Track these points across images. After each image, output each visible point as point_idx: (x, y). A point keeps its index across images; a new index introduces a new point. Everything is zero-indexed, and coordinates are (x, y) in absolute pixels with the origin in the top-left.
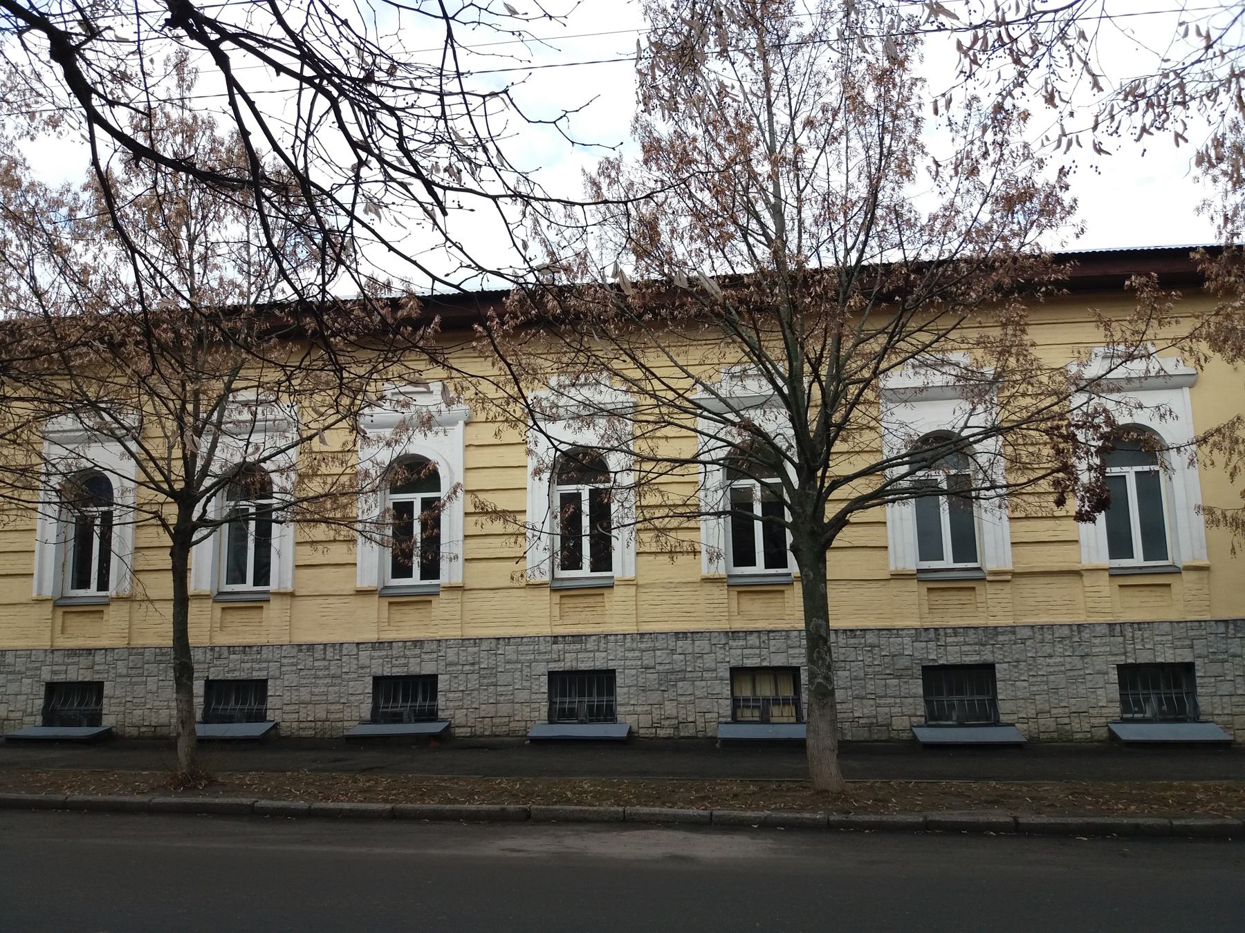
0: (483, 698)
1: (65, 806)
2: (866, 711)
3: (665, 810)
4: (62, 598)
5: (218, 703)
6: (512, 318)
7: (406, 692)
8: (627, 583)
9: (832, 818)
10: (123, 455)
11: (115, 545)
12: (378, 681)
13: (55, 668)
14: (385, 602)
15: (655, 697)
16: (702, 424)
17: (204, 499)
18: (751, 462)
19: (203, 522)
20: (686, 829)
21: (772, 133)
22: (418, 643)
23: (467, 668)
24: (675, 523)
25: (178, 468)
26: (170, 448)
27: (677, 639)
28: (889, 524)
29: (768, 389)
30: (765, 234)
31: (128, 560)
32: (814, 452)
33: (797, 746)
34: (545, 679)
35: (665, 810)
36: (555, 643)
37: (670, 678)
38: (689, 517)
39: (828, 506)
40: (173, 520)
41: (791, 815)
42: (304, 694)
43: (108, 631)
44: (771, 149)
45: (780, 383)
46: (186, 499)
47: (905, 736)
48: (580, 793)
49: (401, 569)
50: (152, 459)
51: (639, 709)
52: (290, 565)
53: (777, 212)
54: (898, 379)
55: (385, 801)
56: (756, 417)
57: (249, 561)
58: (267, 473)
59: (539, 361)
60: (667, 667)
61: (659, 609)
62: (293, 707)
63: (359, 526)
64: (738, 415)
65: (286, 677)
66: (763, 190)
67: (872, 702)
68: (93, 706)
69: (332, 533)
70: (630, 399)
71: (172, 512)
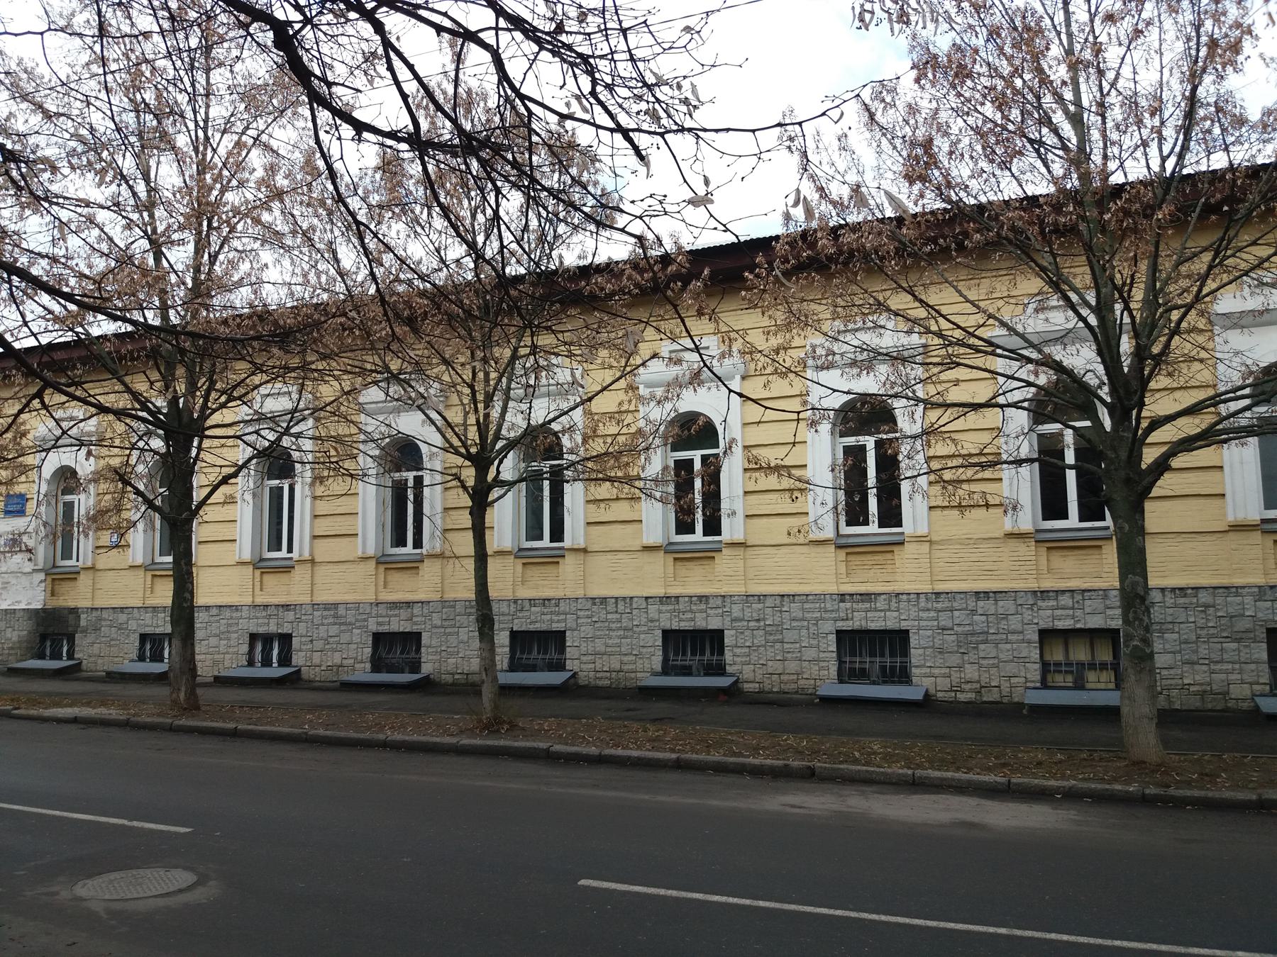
0: (770, 654)
1: (385, 745)
2: (1197, 678)
3: (958, 775)
4: (384, 555)
5: (522, 652)
6: (783, 263)
7: (694, 645)
8: (920, 539)
9: (1147, 791)
10: (423, 422)
11: (426, 509)
12: (667, 634)
13: (380, 619)
14: (670, 558)
15: (955, 660)
16: (1000, 364)
17: (496, 463)
18: (1056, 404)
19: (498, 482)
20: (980, 796)
21: (1070, 35)
22: (703, 598)
23: (752, 624)
24: (970, 473)
25: (473, 434)
26: (466, 414)
27: (978, 599)
28: (1226, 469)
29: (1073, 322)
30: (1065, 148)
31: (439, 522)
32: (1129, 390)
33: (1110, 714)
34: (833, 638)
35: (958, 775)
36: (842, 601)
37: (970, 641)
38: (983, 466)
39: (1145, 450)
40: (471, 482)
41: (1099, 786)
42: (599, 645)
43: (423, 586)
44: (1069, 52)
45: (1084, 312)
46: (482, 461)
47: (1245, 706)
48: (869, 754)
49: (685, 527)
50: (449, 424)
51: (936, 671)
52: (582, 523)
53: (1076, 120)
54: (1228, 303)
55: (673, 751)
56: (1057, 353)
57: (546, 520)
58: (556, 434)
59: (813, 306)
60: (967, 628)
61: (957, 567)
62: (590, 657)
63: (640, 484)
64: (1040, 351)
65: (583, 628)
66: (1060, 99)
67: (1205, 668)
68: (413, 655)
69: (615, 491)
70: (915, 339)
71: (469, 475)
